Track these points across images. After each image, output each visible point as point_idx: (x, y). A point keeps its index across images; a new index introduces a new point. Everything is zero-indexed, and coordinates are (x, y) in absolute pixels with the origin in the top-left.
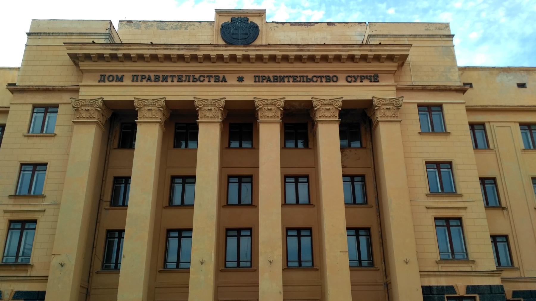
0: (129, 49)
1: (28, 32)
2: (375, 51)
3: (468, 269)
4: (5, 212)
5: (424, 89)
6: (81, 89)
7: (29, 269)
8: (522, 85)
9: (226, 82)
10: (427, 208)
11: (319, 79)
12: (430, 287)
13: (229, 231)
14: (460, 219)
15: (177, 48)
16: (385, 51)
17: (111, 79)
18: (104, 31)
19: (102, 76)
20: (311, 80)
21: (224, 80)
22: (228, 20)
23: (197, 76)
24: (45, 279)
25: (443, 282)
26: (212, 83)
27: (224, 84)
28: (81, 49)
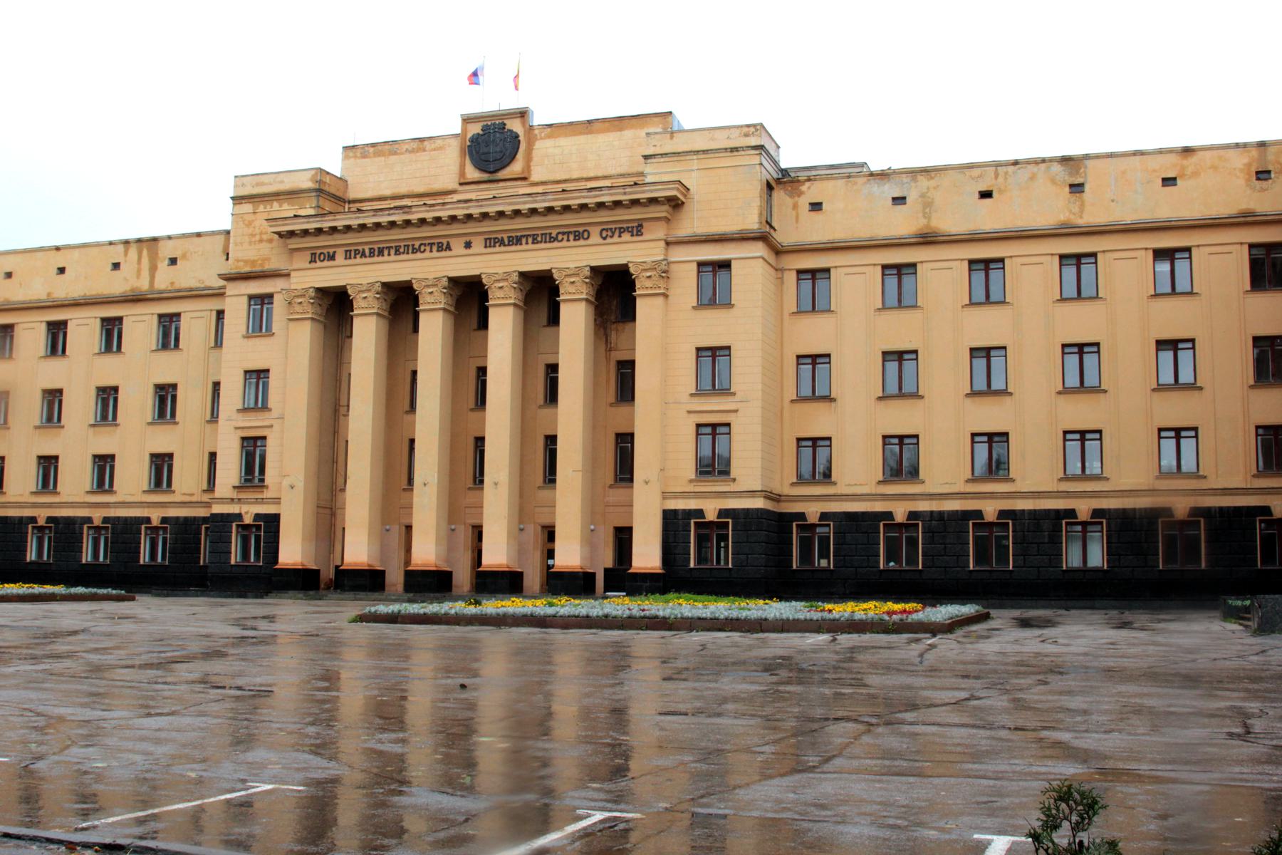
0: (334, 220)
2: (630, 193)
4: (236, 428)
6: (293, 274)
7: (265, 490)
9: (450, 250)
10: (689, 412)
11: (565, 237)
12: (675, 511)
13: (800, 359)
14: (728, 425)
15: (387, 212)
16: (643, 192)
17: (322, 258)
18: (310, 185)
19: (312, 254)
21: (449, 248)
22: (476, 129)
23: (417, 244)
24: (277, 501)
25: (692, 504)
26: (435, 254)
27: (448, 253)
28: (284, 225)
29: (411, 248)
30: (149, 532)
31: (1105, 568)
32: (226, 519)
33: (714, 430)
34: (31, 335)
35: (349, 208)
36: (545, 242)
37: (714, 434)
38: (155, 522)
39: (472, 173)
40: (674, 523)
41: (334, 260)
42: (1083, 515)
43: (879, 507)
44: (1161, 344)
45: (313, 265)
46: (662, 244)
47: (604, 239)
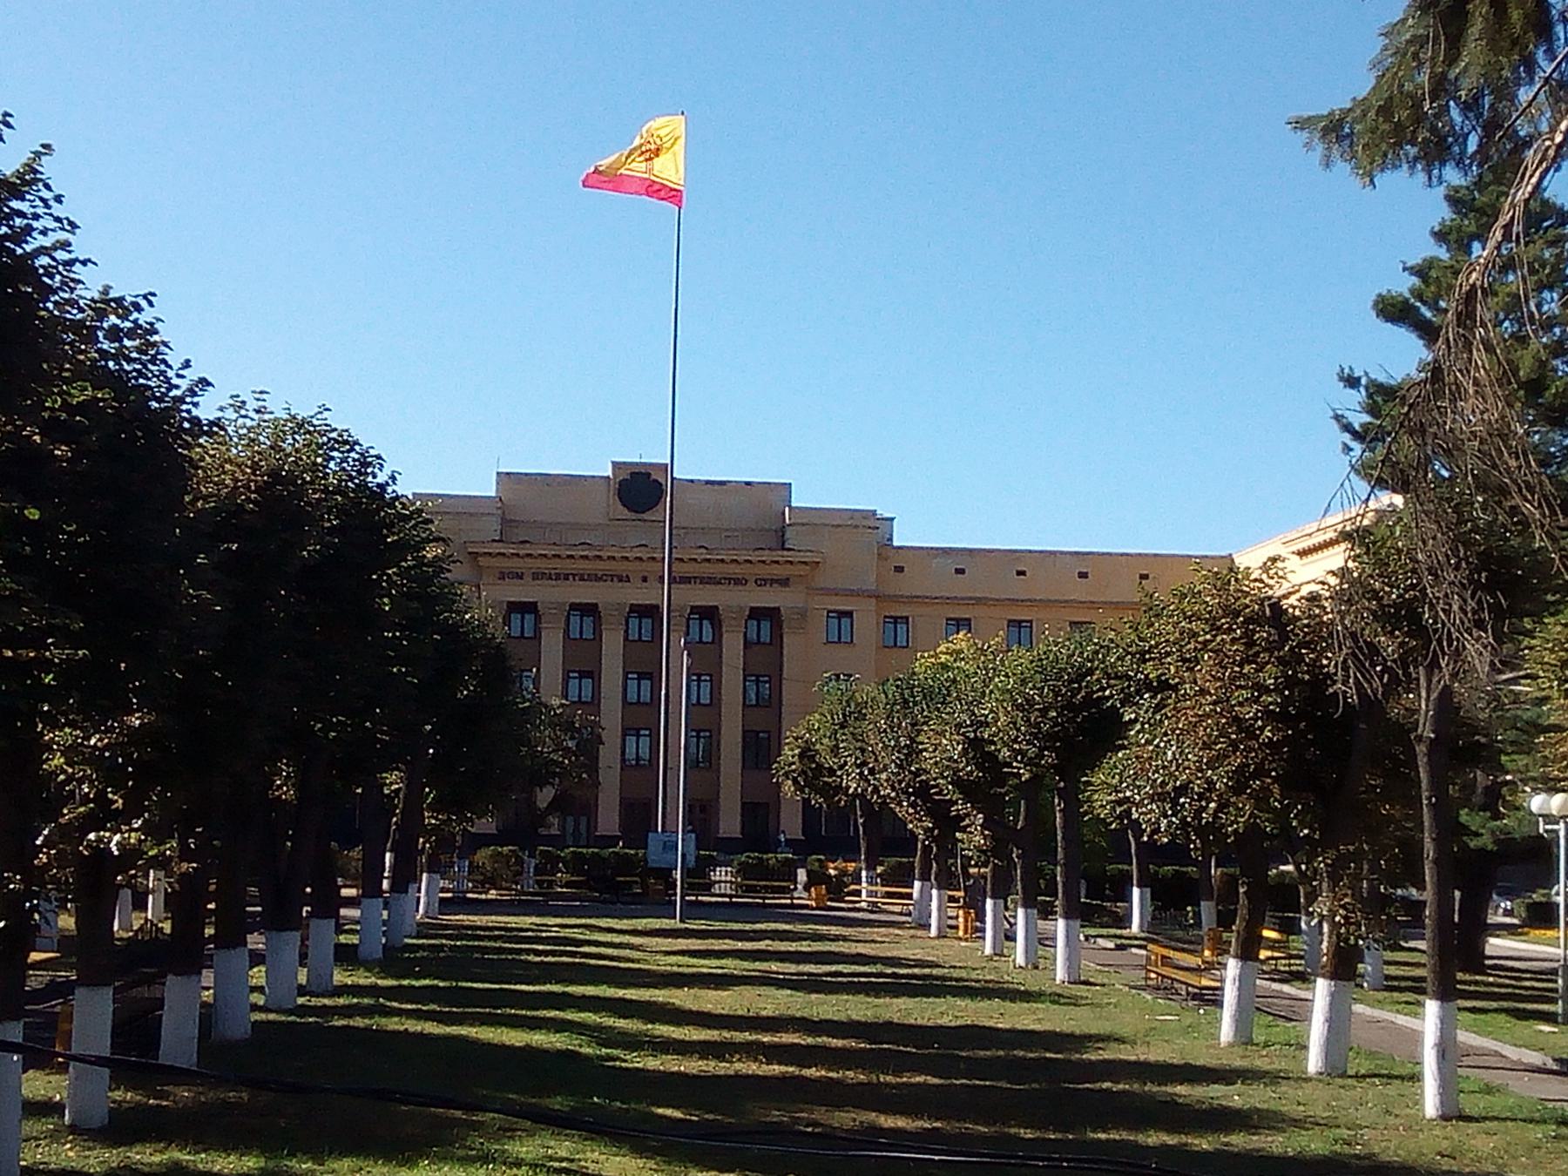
8: (960, 571)
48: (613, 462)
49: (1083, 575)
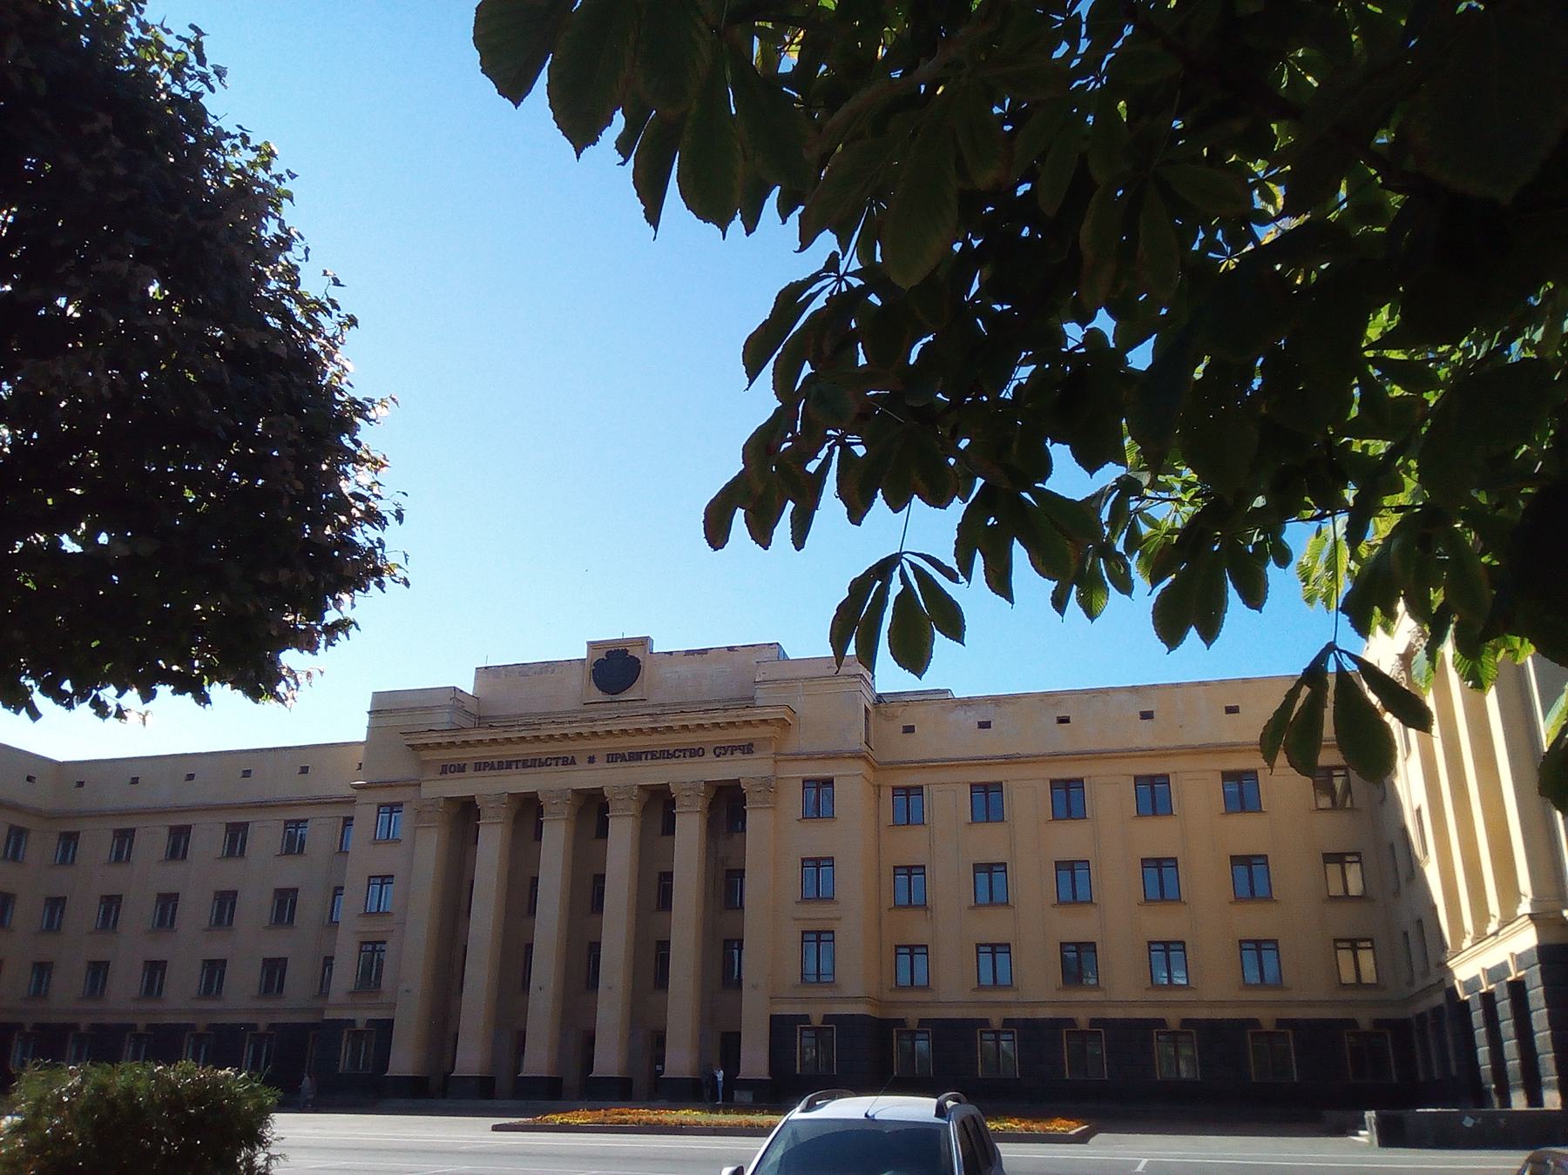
1: (369, 710)
3: (830, 994)
5: (810, 757)
8: (985, 725)
11: (554, 762)
17: (453, 770)
20: (673, 756)
25: (798, 1010)
29: (537, 762)
30: (133, 1039)
31: (1199, 1078)
32: (339, 1024)
33: (818, 937)
34: (40, 848)
35: (479, 724)
36: (664, 758)
37: (818, 941)
38: (262, 1028)
39: (597, 695)
40: (782, 1029)
41: (464, 771)
42: (996, 1023)
43: (975, 1014)
44: (978, 868)
45: (444, 776)
46: (772, 762)
47: (718, 756)
48: (920, 679)
49: (1146, 715)
